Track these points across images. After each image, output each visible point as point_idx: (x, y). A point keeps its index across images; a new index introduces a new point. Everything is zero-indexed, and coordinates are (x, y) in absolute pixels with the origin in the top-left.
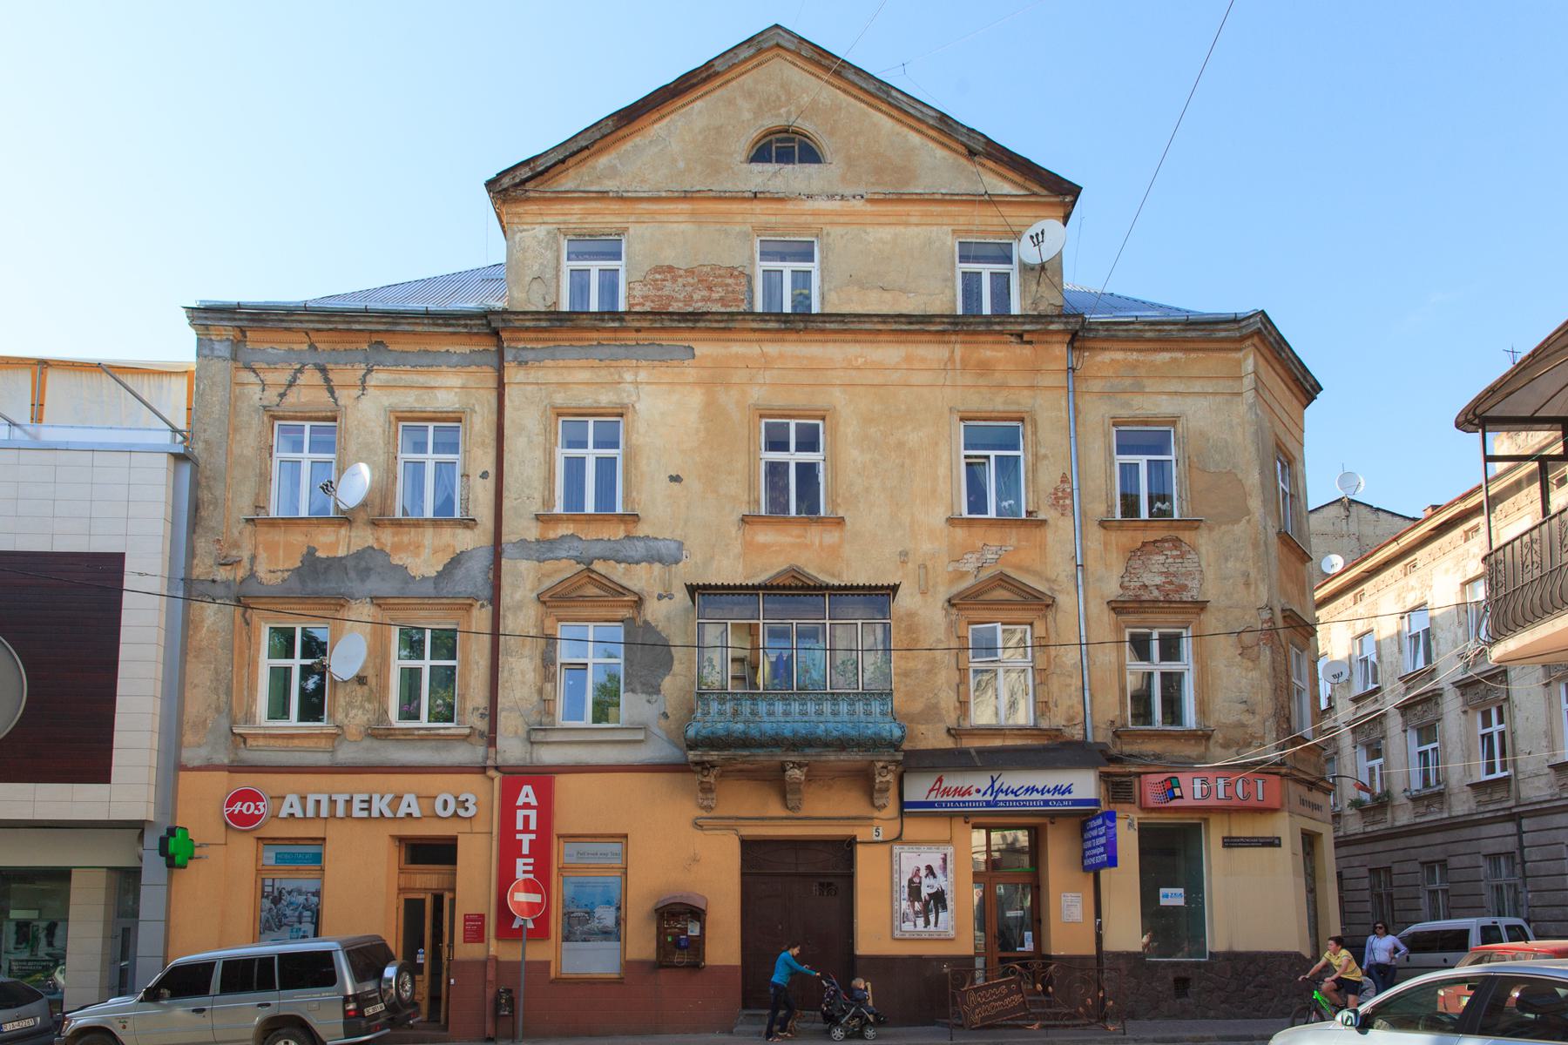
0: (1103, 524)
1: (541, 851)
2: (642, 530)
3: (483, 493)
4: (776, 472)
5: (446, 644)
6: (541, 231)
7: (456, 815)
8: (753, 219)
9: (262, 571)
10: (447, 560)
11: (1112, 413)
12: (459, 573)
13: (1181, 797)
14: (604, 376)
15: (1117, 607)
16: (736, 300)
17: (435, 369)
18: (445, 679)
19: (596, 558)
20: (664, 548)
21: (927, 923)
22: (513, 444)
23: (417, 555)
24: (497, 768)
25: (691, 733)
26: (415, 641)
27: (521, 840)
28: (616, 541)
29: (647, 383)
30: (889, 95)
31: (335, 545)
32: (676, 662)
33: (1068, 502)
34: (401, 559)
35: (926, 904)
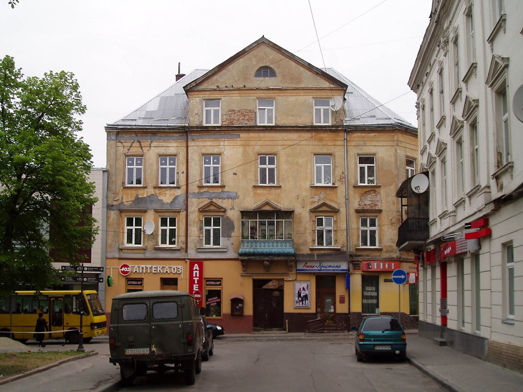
0: (355, 187)
1: (200, 282)
2: (226, 189)
3: (183, 177)
4: (263, 171)
5: (173, 222)
6: (198, 99)
7: (176, 273)
8: (256, 95)
9: (124, 201)
10: (173, 198)
11: (357, 152)
12: (177, 201)
13: (371, 268)
14: (215, 143)
15: (357, 211)
16: (251, 120)
17: (169, 141)
18: (173, 232)
19: (214, 198)
20: (232, 195)
21: (303, 303)
22: (191, 164)
23: (165, 196)
24: (188, 259)
25: (240, 251)
26: (139, 198)
27: (195, 280)
28: (219, 193)
29: (227, 145)
30: (294, 57)
31: (143, 194)
32: (235, 228)
33: (344, 180)
34: (161, 198)
35: (302, 298)
